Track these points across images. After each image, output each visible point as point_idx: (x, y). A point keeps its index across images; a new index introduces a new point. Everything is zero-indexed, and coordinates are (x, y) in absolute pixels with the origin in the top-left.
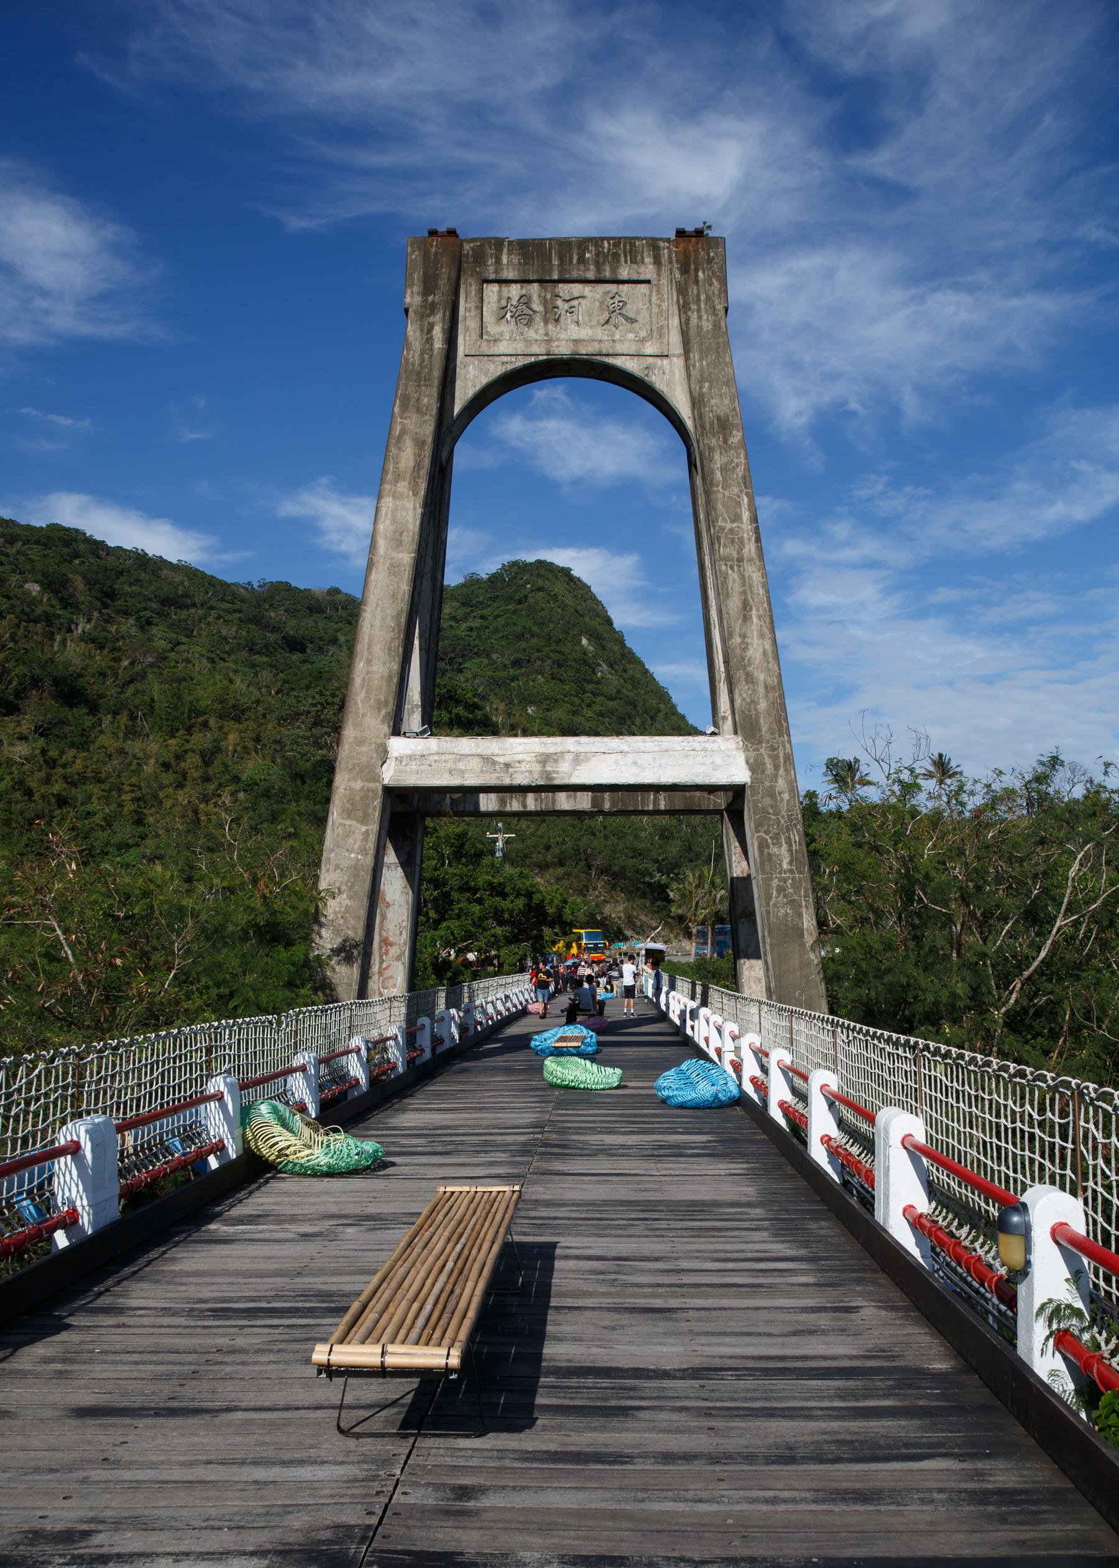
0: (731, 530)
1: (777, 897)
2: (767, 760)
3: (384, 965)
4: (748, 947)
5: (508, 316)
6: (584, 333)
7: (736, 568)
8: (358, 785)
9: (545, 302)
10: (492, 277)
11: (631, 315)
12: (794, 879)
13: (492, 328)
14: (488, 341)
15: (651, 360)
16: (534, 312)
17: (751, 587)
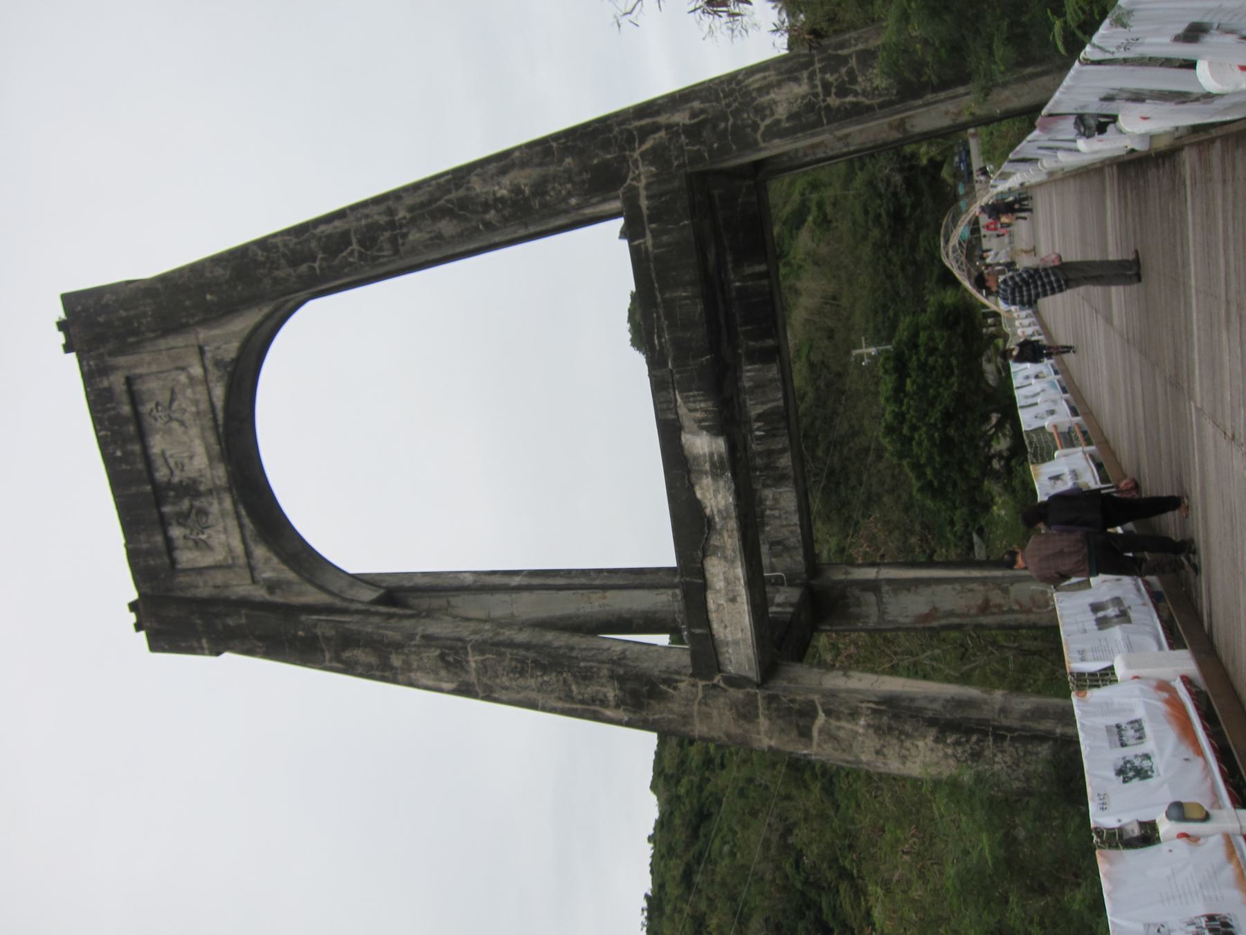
0: (361, 243)
1: (856, 94)
2: (648, 144)
3: (1016, 607)
4: (947, 113)
5: (203, 537)
6: (199, 448)
7: (405, 230)
8: (763, 723)
9: (179, 498)
10: (166, 560)
11: (167, 395)
12: (823, 71)
13: (219, 556)
14: (233, 558)
15: (208, 363)
16: (192, 506)
17: (422, 205)
